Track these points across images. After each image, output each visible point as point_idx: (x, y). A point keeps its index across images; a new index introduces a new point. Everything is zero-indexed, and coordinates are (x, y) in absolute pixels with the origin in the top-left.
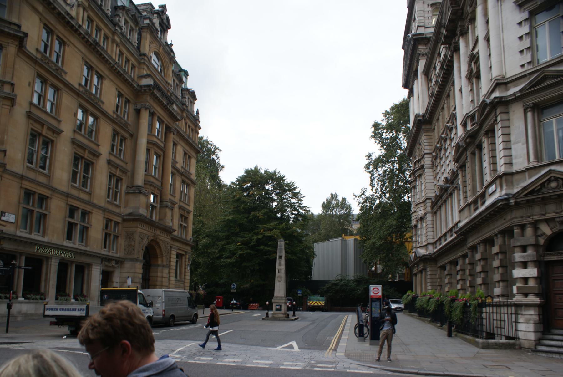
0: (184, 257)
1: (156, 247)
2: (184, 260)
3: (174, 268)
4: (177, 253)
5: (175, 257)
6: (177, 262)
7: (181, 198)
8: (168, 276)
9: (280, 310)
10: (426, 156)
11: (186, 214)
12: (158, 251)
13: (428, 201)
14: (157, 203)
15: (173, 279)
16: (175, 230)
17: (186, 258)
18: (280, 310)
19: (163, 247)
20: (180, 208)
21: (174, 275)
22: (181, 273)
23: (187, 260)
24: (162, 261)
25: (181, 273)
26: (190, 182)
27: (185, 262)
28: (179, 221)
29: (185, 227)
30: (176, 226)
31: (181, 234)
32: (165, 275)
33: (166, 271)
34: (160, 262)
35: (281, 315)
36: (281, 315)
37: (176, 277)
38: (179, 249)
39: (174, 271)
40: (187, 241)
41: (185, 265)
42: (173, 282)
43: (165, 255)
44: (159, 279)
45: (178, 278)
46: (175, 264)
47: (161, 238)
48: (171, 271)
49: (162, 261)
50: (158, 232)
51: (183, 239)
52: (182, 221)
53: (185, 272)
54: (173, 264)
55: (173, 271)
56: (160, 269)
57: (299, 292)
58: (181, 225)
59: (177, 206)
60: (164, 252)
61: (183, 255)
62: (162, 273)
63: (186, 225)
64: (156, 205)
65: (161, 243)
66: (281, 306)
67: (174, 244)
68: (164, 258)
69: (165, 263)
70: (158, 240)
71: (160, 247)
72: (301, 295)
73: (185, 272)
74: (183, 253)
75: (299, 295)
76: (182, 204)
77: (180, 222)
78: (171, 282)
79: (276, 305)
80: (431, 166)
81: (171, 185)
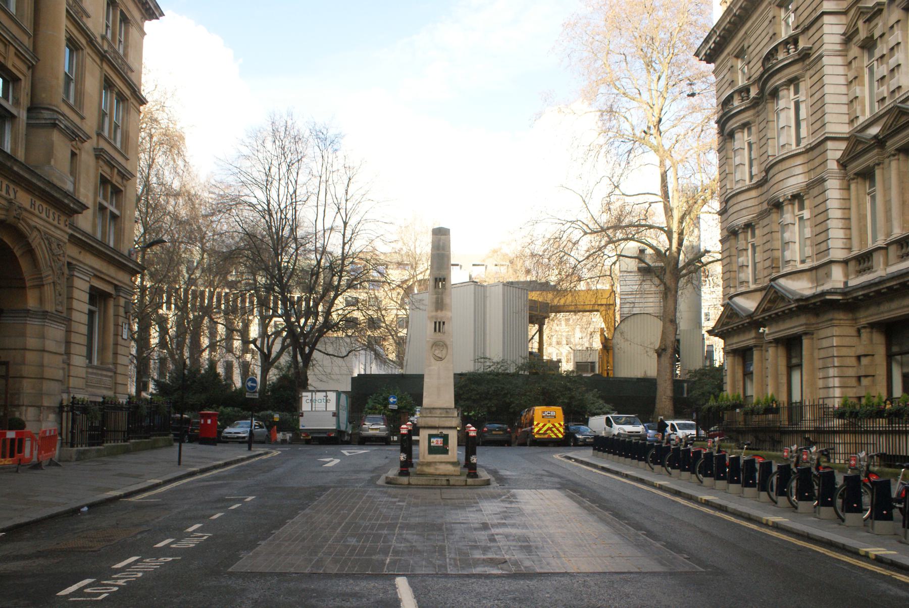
0: (111, 303)
1: (18, 253)
2: (111, 311)
3: (84, 329)
4: (92, 288)
5: (86, 297)
6: (91, 313)
7: (101, 127)
8: (62, 350)
9: (443, 450)
10: (827, 19)
11: (116, 179)
12: (25, 265)
13: (830, 145)
14: (17, 103)
15: (79, 361)
16: (84, 207)
17: (117, 306)
18: (443, 450)
19: (41, 253)
20: (99, 154)
21: (84, 350)
22: (102, 349)
23: (122, 311)
24: (41, 300)
25: (102, 349)
26: (127, 92)
27: (117, 315)
28: (96, 194)
29: (114, 217)
30: (87, 193)
31: (104, 233)
32: (50, 345)
33: (55, 332)
34: (32, 303)
35: (450, 469)
36: (450, 469)
37: (89, 356)
38: (96, 276)
39: (83, 340)
40: (122, 255)
41: (117, 325)
42: (82, 372)
43: (50, 280)
44: (30, 357)
45: (95, 362)
46: (85, 319)
47: (35, 221)
48: (75, 338)
49: (41, 300)
50: (23, 199)
51: (107, 246)
52: (105, 198)
53: (116, 344)
54: (80, 317)
55: (80, 339)
56: (33, 326)
57: (392, 400)
58: (102, 208)
59: (88, 146)
60: (46, 272)
61: (109, 295)
62: (43, 337)
63: (117, 212)
64: (14, 111)
65: (35, 240)
66: (445, 438)
67: (81, 257)
68: (48, 290)
69: (50, 307)
70: (22, 226)
71: (30, 252)
72: (395, 407)
73: (116, 344)
74: (112, 292)
75: (391, 407)
76: (103, 145)
77: (100, 199)
78: (74, 371)
79: (431, 436)
80: (838, 47)
81: (68, 79)
